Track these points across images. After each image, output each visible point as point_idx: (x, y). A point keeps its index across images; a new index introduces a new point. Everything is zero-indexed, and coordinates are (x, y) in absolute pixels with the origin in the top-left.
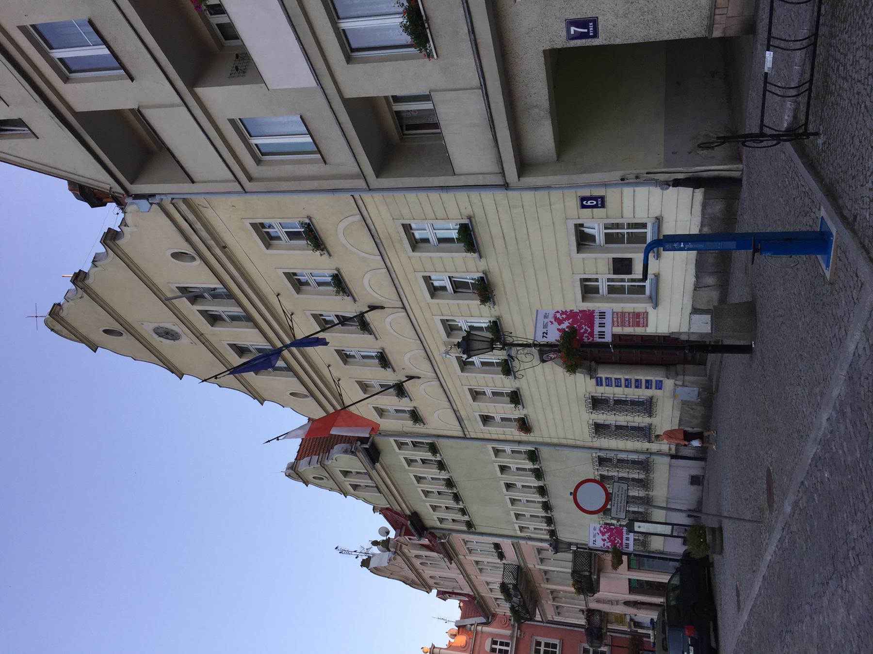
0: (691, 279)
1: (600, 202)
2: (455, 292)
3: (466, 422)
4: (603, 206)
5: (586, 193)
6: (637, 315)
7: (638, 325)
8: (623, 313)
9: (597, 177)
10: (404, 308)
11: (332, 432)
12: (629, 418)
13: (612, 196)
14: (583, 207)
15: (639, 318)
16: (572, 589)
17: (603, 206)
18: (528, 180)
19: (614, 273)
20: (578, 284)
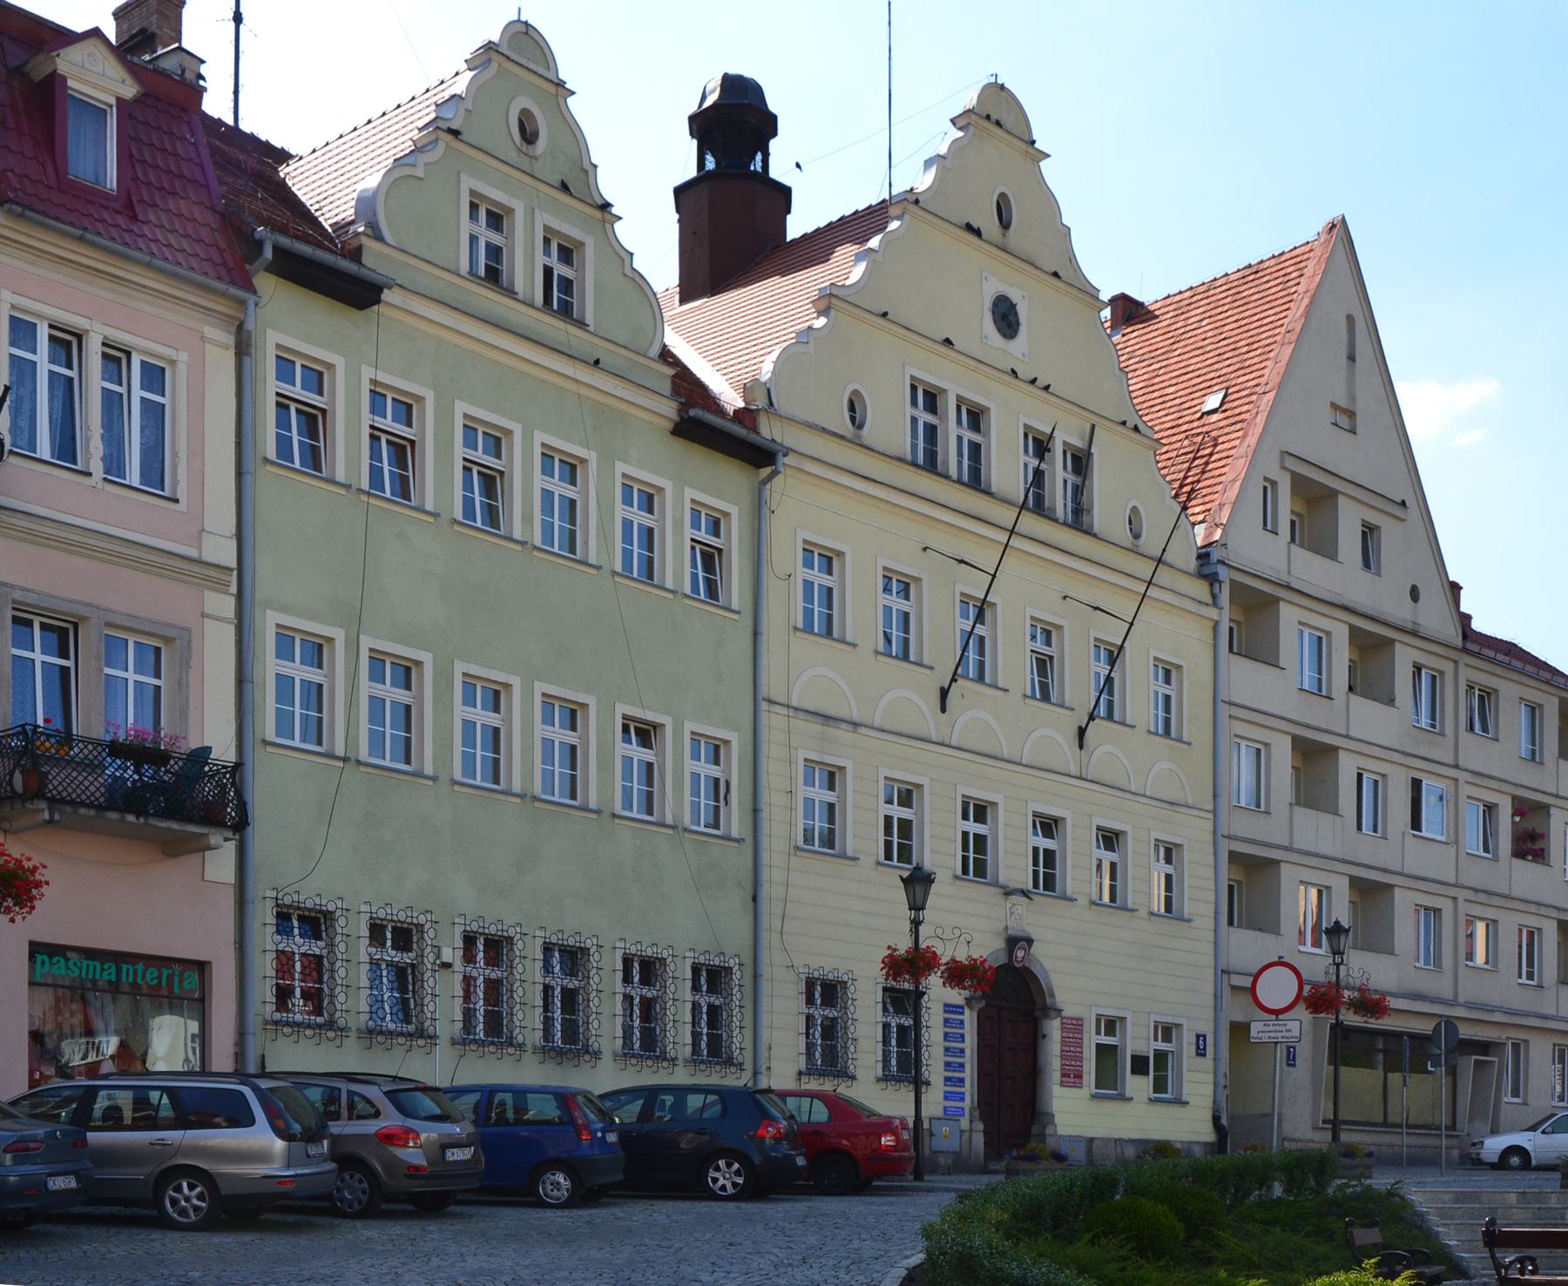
0: (1125, 1135)
1: (1201, 1052)
2: (128, 354)
3: (818, 728)
4: (1198, 1054)
5: (1210, 1040)
6: (1079, 1076)
7: (1063, 1075)
8: (1081, 1059)
9: (1225, 1054)
10: (1215, 812)
11: (112, 180)
12: (863, 1044)
13: (1207, 1062)
14: (1198, 1037)
15: (1072, 1077)
16: (70, 83)
17: (1198, 1054)
18: (1227, 990)
19: (1133, 1057)
20: (1121, 1014)
